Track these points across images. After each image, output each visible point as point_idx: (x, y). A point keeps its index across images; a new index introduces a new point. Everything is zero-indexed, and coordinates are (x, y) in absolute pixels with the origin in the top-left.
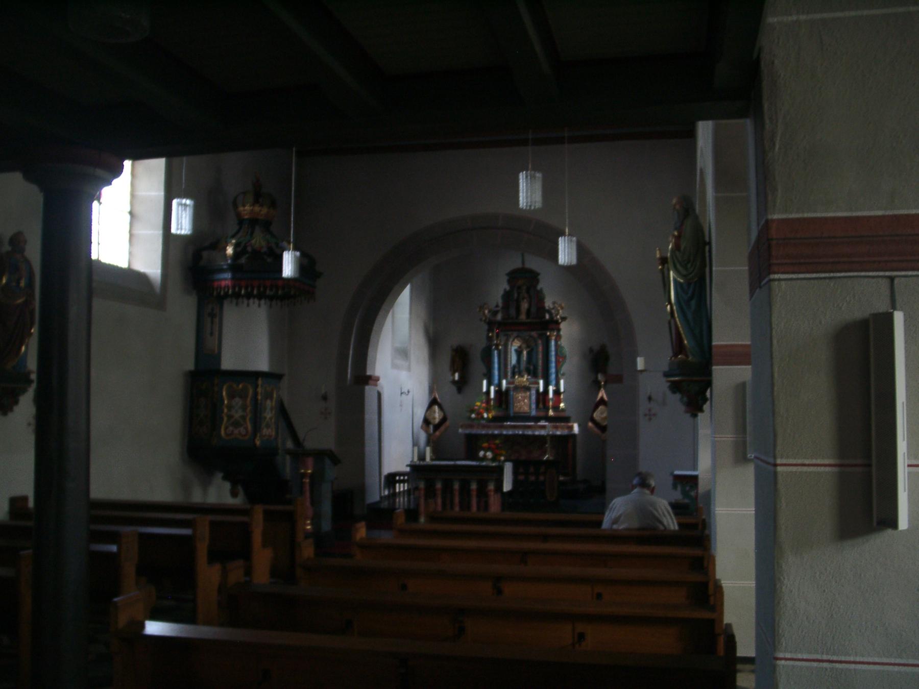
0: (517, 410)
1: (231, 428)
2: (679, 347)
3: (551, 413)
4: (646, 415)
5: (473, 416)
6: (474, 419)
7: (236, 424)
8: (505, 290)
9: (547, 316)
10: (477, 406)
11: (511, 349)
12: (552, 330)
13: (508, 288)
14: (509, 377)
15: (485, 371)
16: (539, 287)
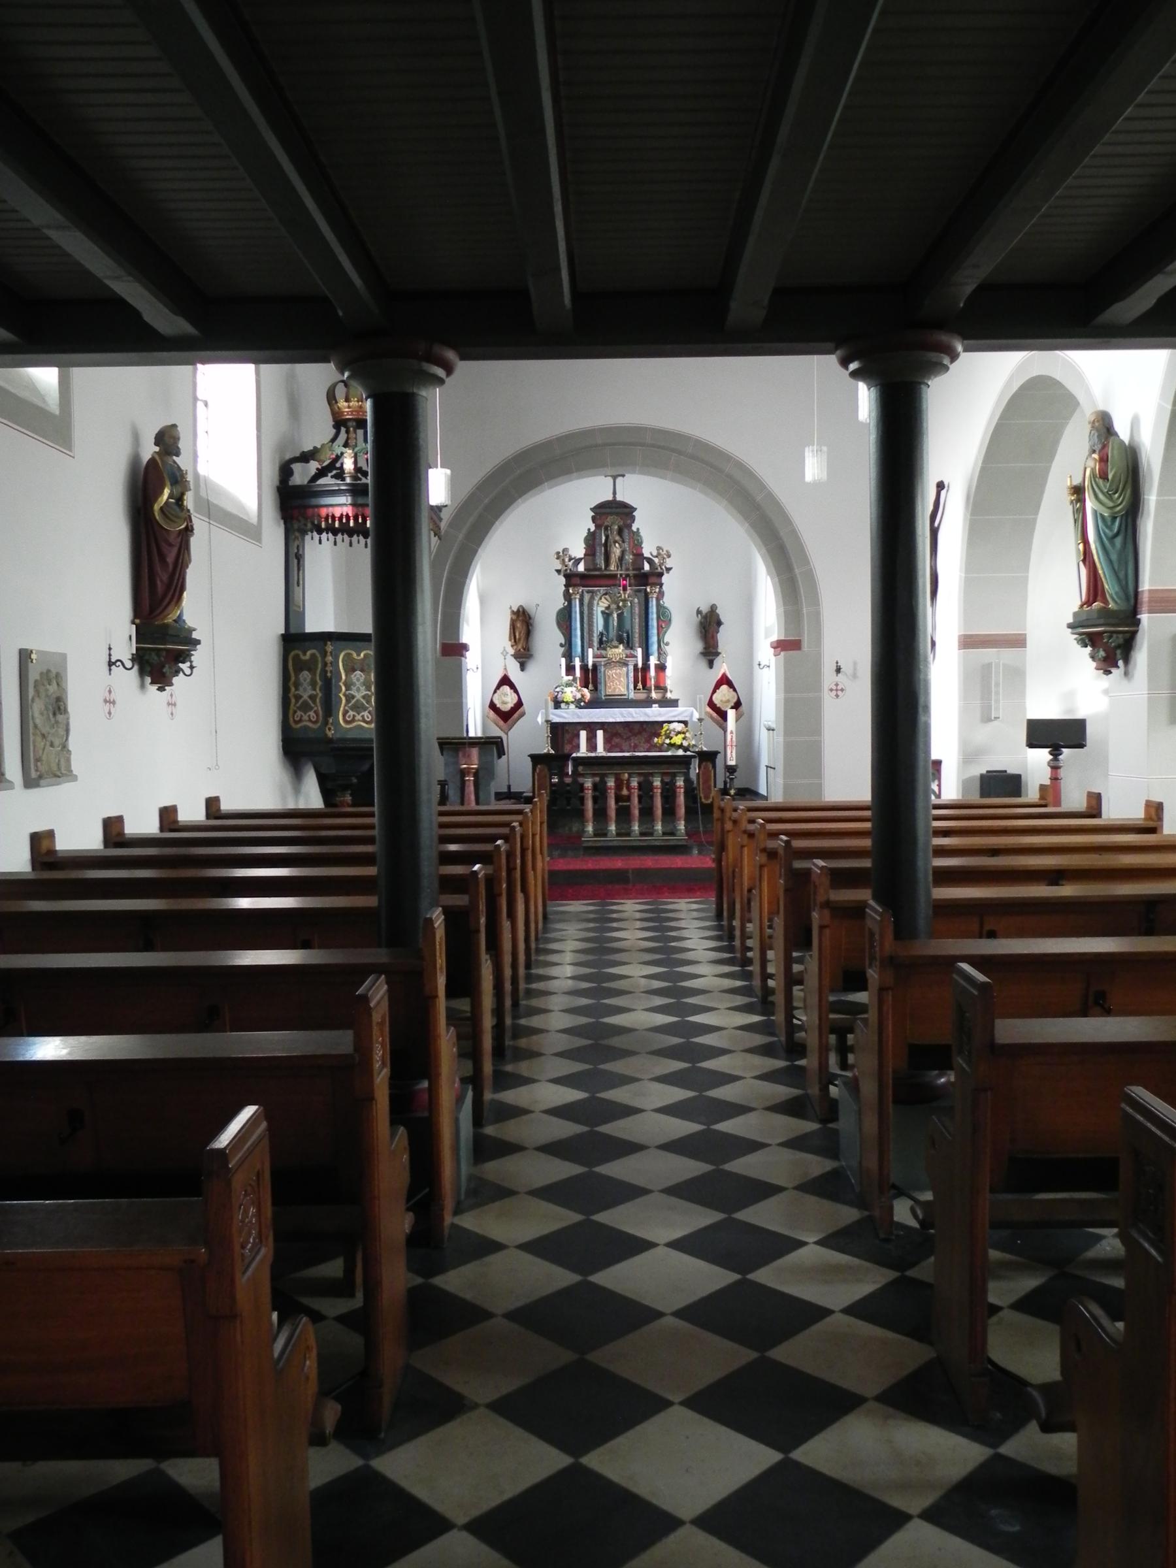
0: (609, 692)
1: (351, 713)
2: (1095, 590)
4: (831, 690)
7: (358, 708)
9: (647, 567)
11: (597, 610)
12: (653, 585)
13: (593, 528)
16: (634, 528)
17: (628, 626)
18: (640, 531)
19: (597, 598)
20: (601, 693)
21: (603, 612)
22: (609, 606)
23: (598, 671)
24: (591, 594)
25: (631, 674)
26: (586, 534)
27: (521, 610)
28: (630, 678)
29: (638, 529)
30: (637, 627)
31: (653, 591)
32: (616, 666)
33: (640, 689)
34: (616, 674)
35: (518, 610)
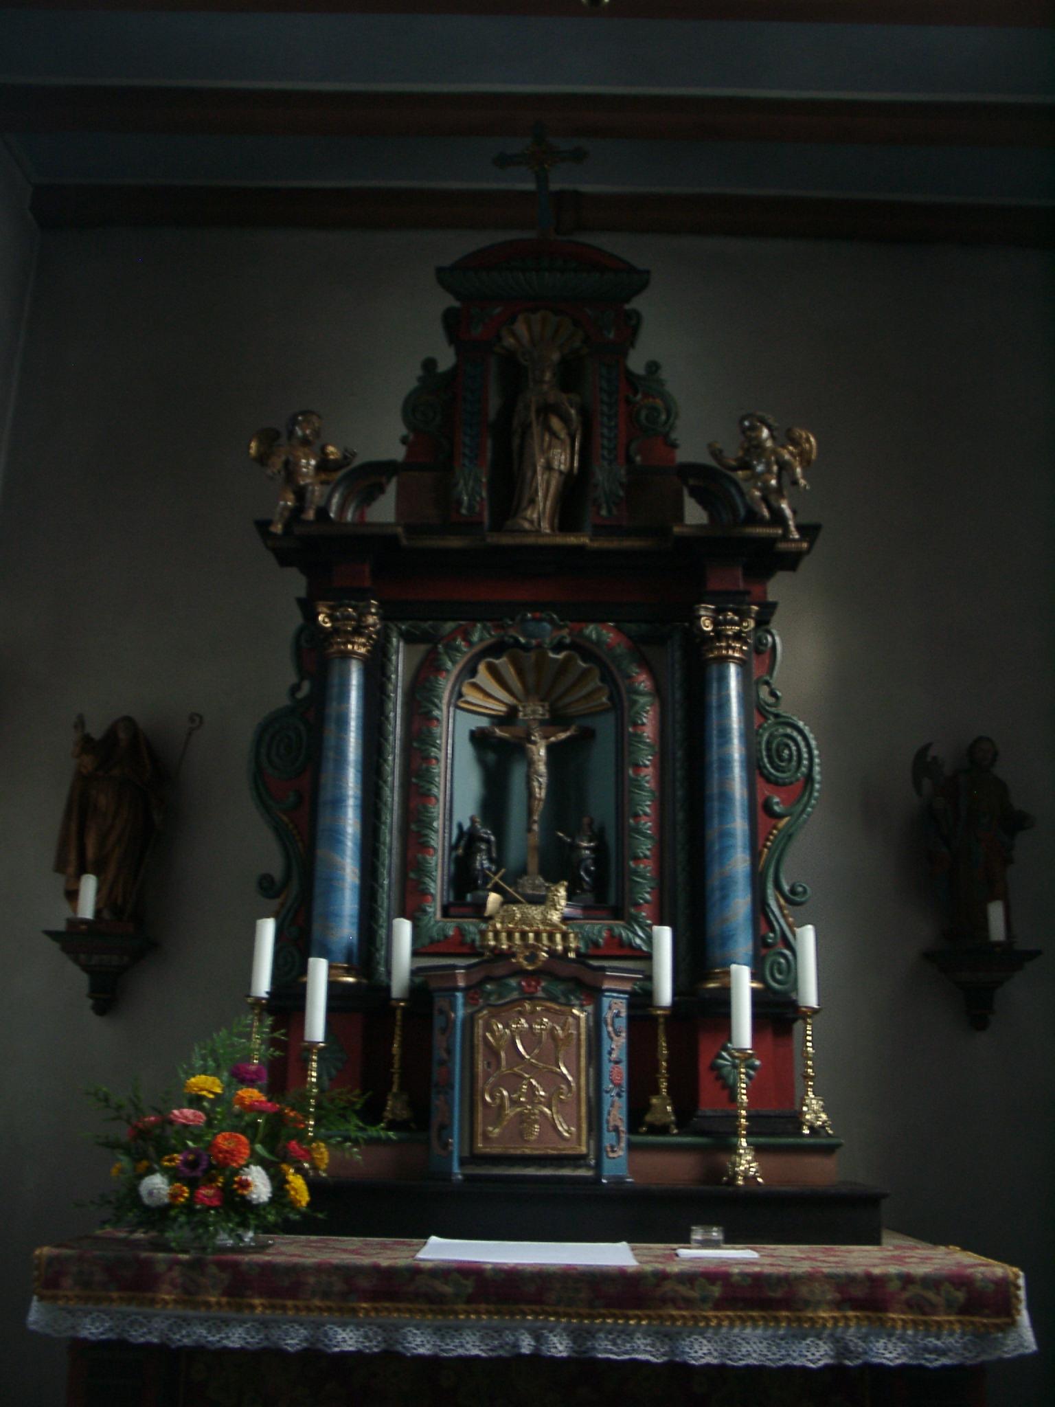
3: (746, 1163)
5: (157, 1185)
6: (158, 1216)
8: (429, 365)
10: (196, 1101)
12: (728, 601)
14: (434, 909)
15: (274, 864)
16: (636, 362)
17: (600, 804)
18: (664, 374)
19: (453, 669)
20: (446, 1145)
21: (479, 739)
22: (512, 711)
23: (438, 1022)
24: (422, 648)
25: (616, 1046)
26: (413, 384)
27: (122, 735)
28: (607, 1067)
29: (653, 367)
30: (647, 807)
31: (731, 630)
32: (532, 998)
33: (663, 1130)
34: (531, 1039)
35: (112, 733)
